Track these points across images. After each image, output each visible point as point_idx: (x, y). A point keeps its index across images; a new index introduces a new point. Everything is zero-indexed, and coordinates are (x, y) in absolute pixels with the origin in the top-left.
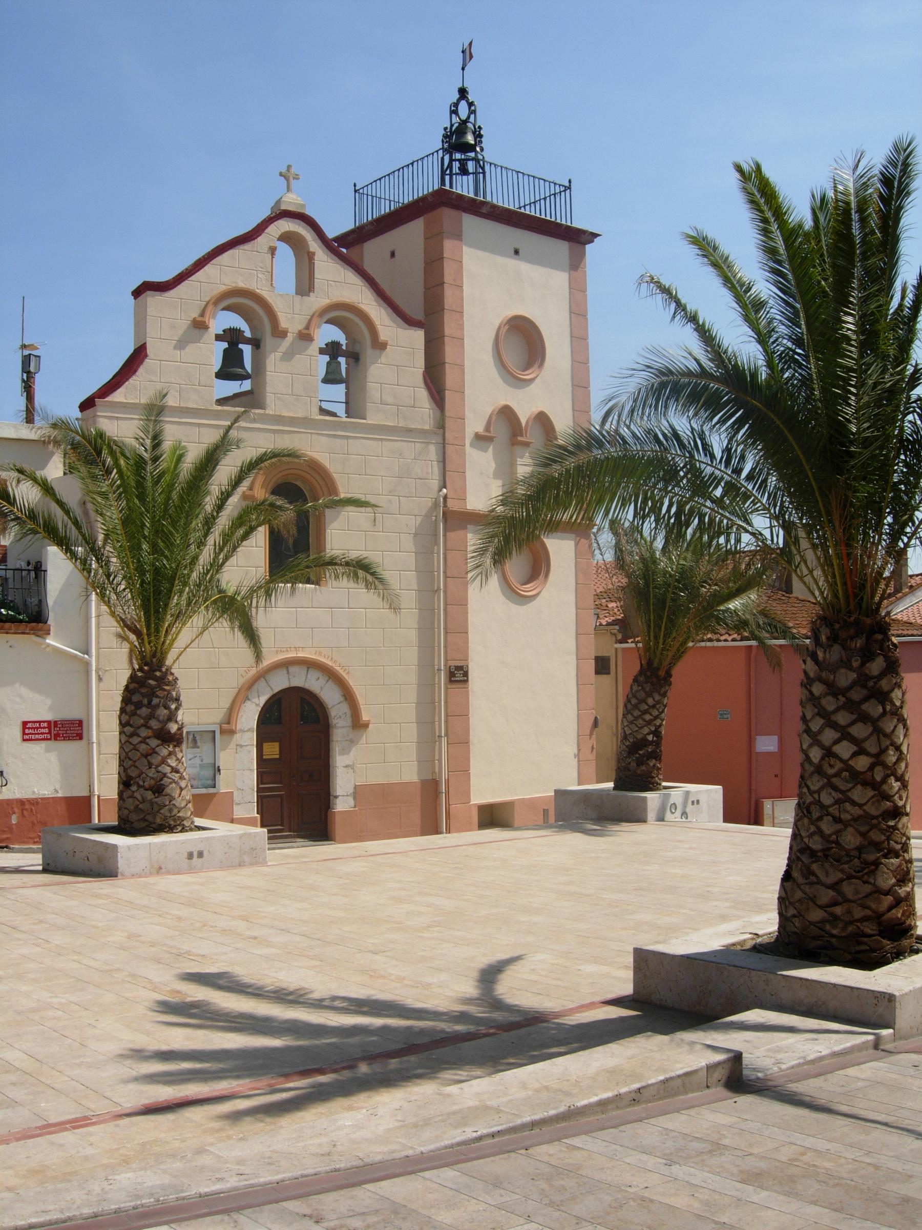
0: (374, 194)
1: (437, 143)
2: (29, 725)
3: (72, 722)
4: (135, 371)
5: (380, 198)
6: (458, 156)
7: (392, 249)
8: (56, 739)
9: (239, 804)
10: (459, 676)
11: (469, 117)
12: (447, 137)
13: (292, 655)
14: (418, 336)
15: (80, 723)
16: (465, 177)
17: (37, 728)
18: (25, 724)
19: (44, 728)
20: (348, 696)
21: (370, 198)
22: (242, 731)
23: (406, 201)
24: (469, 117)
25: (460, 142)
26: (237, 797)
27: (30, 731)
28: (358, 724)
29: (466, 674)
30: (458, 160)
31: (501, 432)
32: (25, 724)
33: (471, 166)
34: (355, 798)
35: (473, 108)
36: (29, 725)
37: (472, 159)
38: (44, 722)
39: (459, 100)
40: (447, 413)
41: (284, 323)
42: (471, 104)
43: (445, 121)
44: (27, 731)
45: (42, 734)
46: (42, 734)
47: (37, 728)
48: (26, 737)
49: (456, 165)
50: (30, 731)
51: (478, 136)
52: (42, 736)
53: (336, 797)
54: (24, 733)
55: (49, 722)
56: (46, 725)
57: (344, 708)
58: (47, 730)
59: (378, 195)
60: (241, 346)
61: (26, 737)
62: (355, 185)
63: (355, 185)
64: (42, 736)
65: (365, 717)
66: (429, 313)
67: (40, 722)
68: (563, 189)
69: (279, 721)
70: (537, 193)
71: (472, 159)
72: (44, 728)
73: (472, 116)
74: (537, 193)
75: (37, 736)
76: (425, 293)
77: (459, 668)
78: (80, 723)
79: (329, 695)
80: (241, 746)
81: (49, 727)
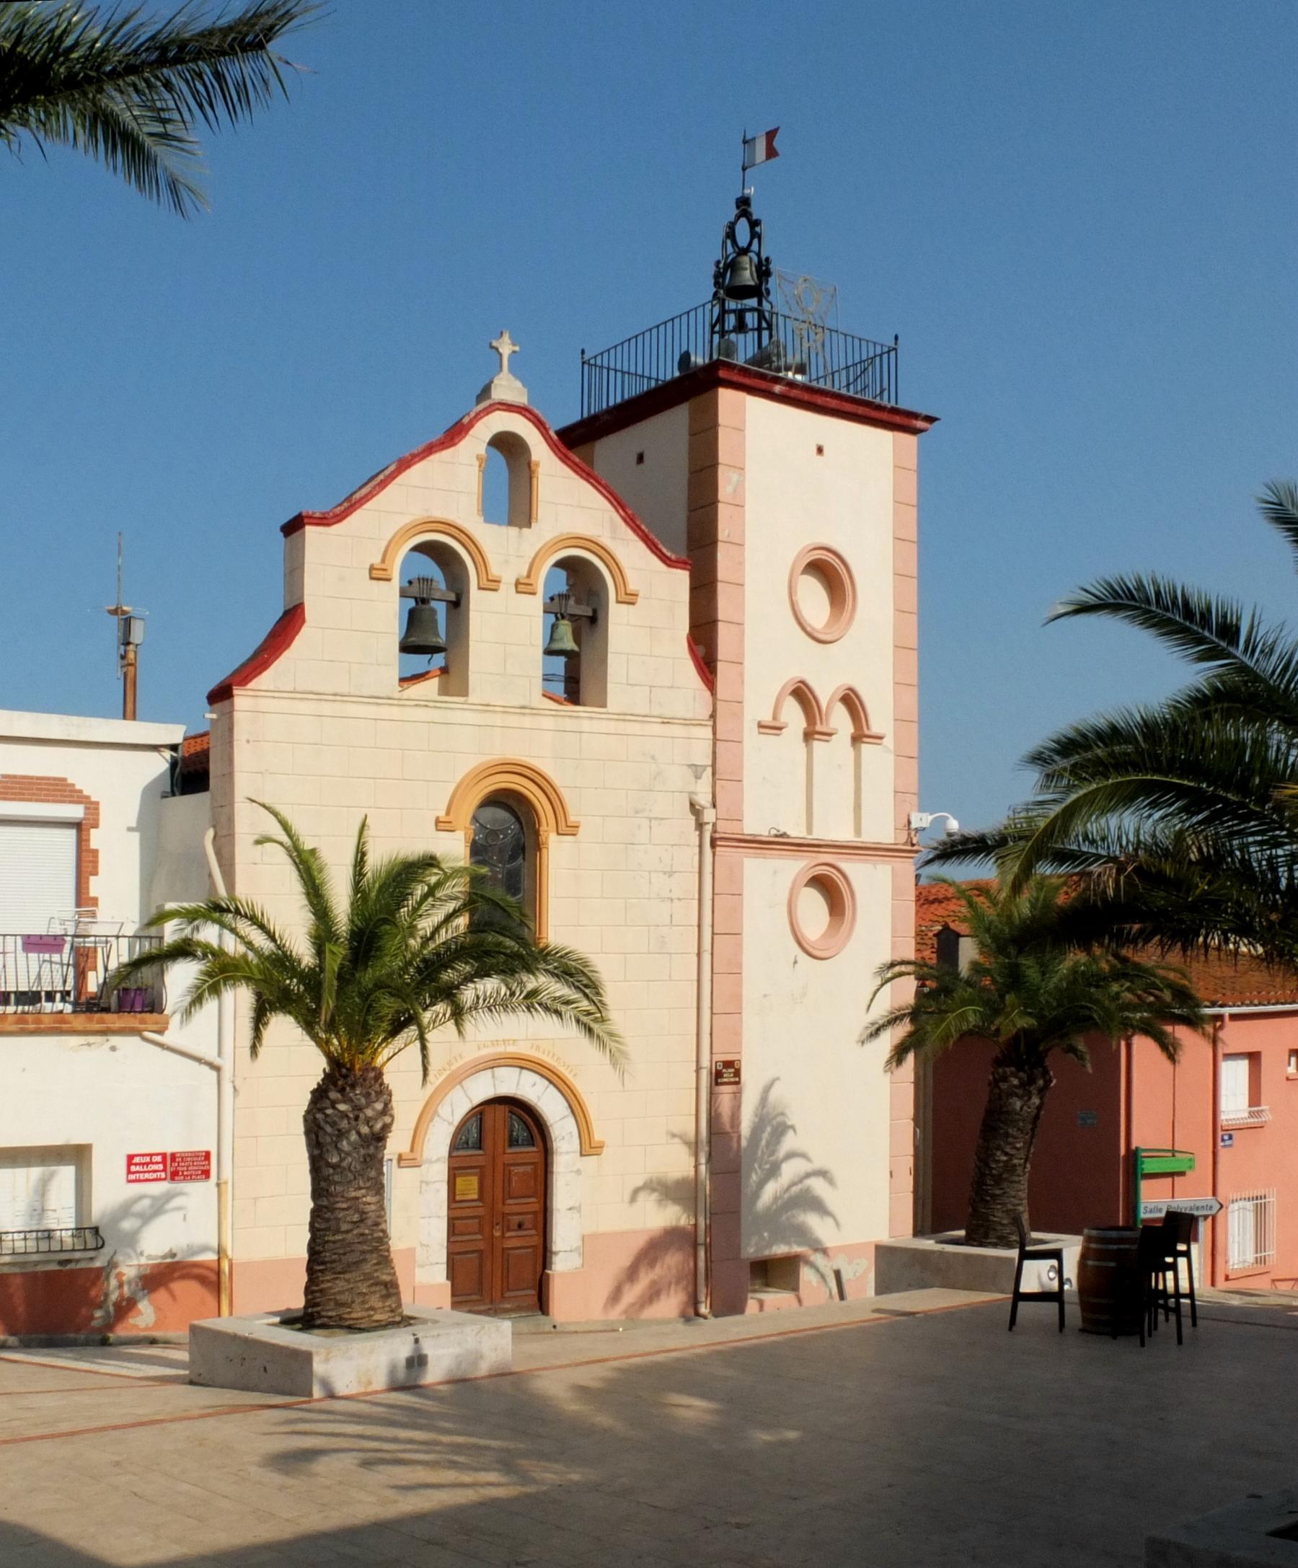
0: (619, 367)
1: (707, 289)
2: (137, 1160)
3: (195, 1155)
4: (289, 645)
5: (602, 367)
6: (732, 304)
7: (639, 450)
8: (173, 1179)
9: (422, 1266)
10: (728, 1075)
11: (750, 244)
12: (719, 276)
13: (501, 1049)
14: (681, 579)
15: (207, 1155)
16: (741, 336)
17: (147, 1164)
18: (130, 1158)
19: (157, 1163)
20: (576, 1108)
21: (612, 373)
22: (430, 1162)
23: (669, 377)
24: (750, 244)
25: (741, 285)
26: (420, 1255)
27: (138, 1168)
28: (589, 1147)
29: (737, 1073)
30: (734, 311)
31: (793, 715)
32: (130, 1158)
33: (751, 319)
34: (583, 1255)
35: (757, 229)
36: (137, 1160)
37: (752, 310)
38: (157, 1154)
39: (738, 217)
40: (719, 696)
41: (495, 571)
42: (754, 224)
43: (712, 251)
44: (133, 1168)
45: (155, 1171)
46: (155, 1171)
47: (147, 1164)
48: (132, 1177)
49: (731, 321)
50: (138, 1168)
51: (763, 271)
52: (154, 1176)
53: (556, 1253)
54: (129, 1172)
55: (164, 1155)
56: (159, 1159)
57: (529, 1077)
58: (161, 1167)
59: (647, 374)
60: (433, 604)
61: (132, 1177)
62: (583, 352)
63: (583, 352)
64: (154, 1176)
65: (598, 1136)
66: (694, 542)
67: (151, 1155)
68: (886, 349)
69: (479, 1145)
70: (842, 355)
71: (752, 310)
72: (157, 1163)
73: (756, 241)
74: (835, 360)
75: (147, 1176)
76: (689, 519)
77: (728, 1064)
78: (207, 1155)
79: (550, 1106)
80: (427, 1183)
81: (164, 1162)
